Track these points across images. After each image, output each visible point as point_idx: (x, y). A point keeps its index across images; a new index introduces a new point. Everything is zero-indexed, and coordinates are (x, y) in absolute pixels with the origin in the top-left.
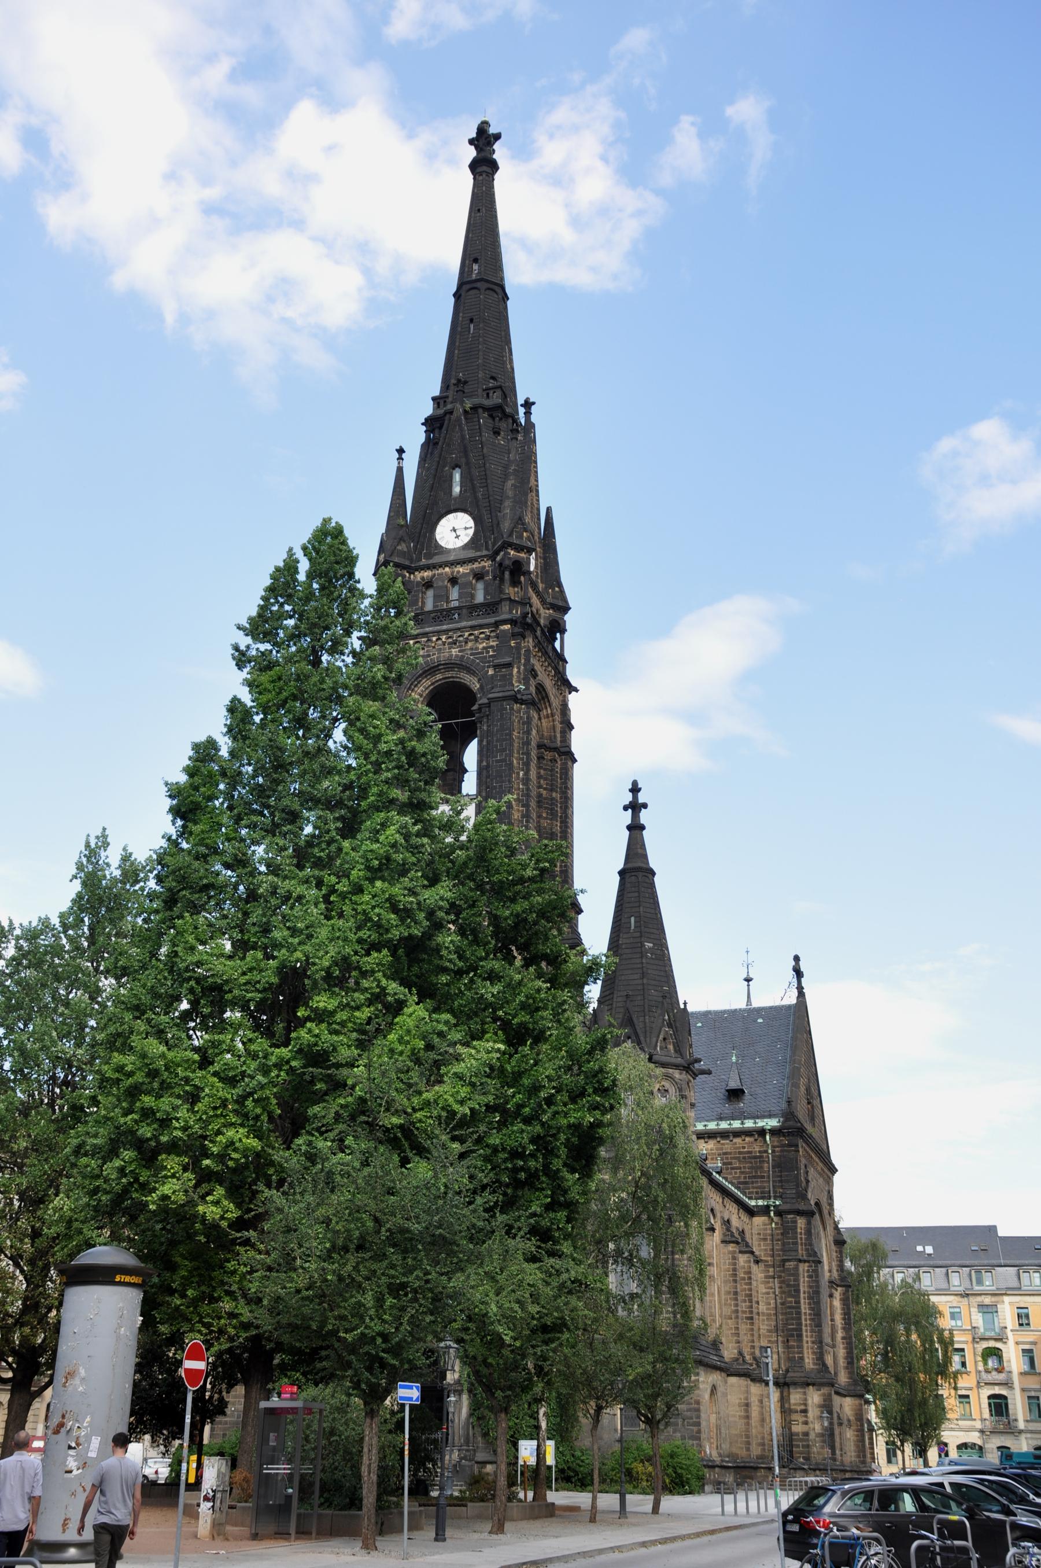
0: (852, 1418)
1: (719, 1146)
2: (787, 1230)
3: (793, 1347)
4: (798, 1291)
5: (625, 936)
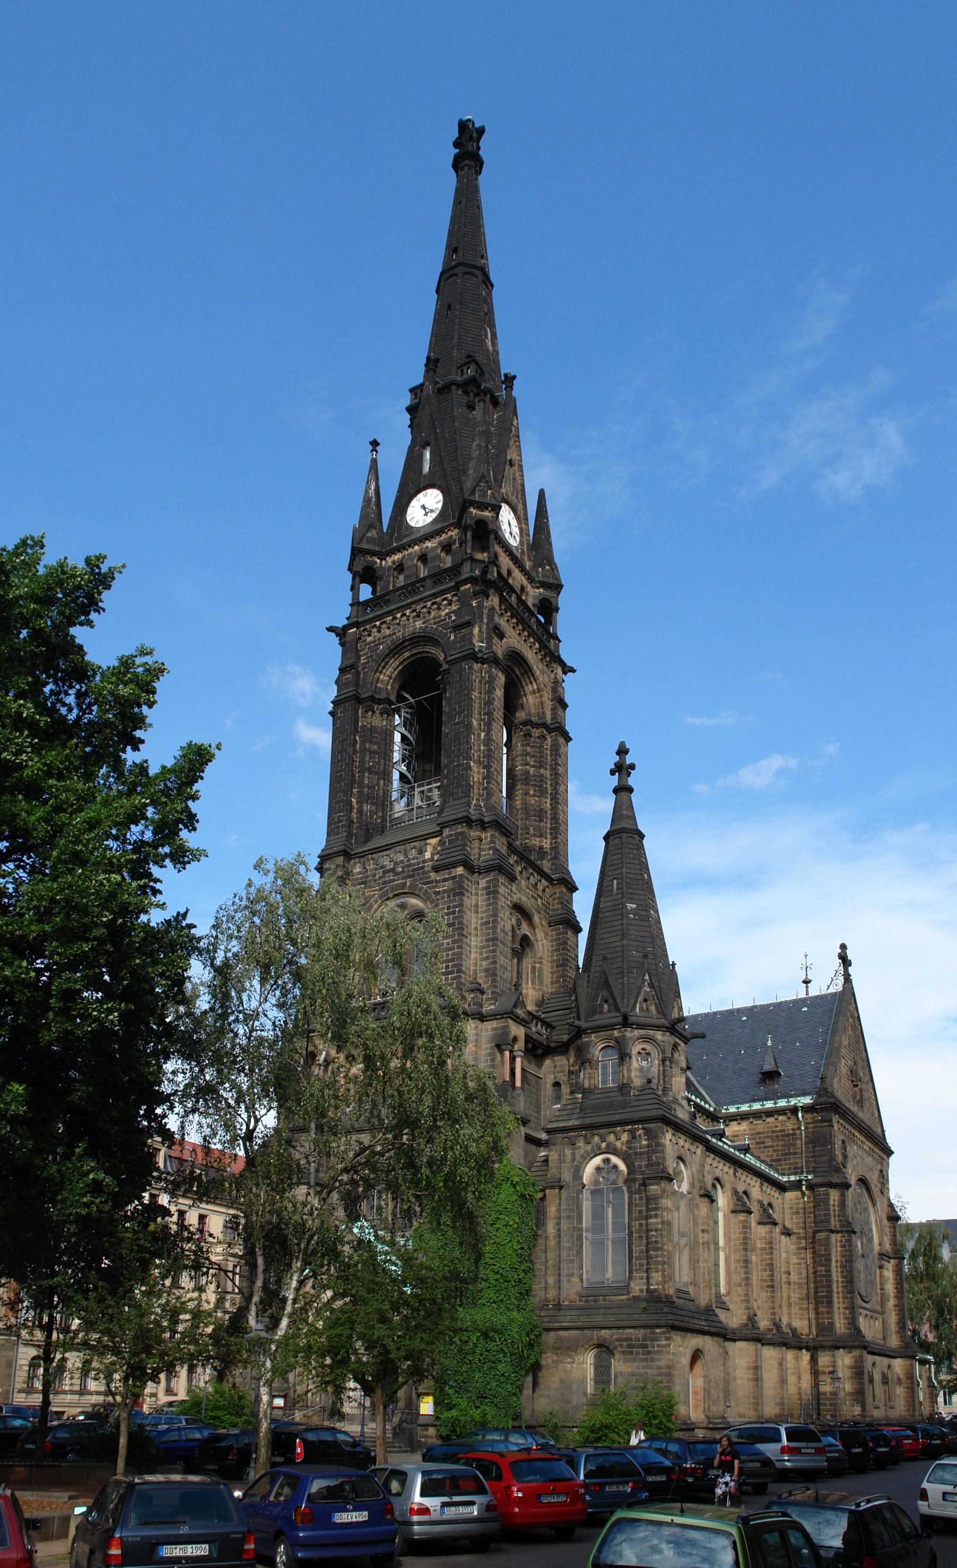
0: (902, 1377)
1: (752, 1127)
2: (820, 1203)
3: (823, 1313)
4: (829, 1260)
5: (607, 899)
